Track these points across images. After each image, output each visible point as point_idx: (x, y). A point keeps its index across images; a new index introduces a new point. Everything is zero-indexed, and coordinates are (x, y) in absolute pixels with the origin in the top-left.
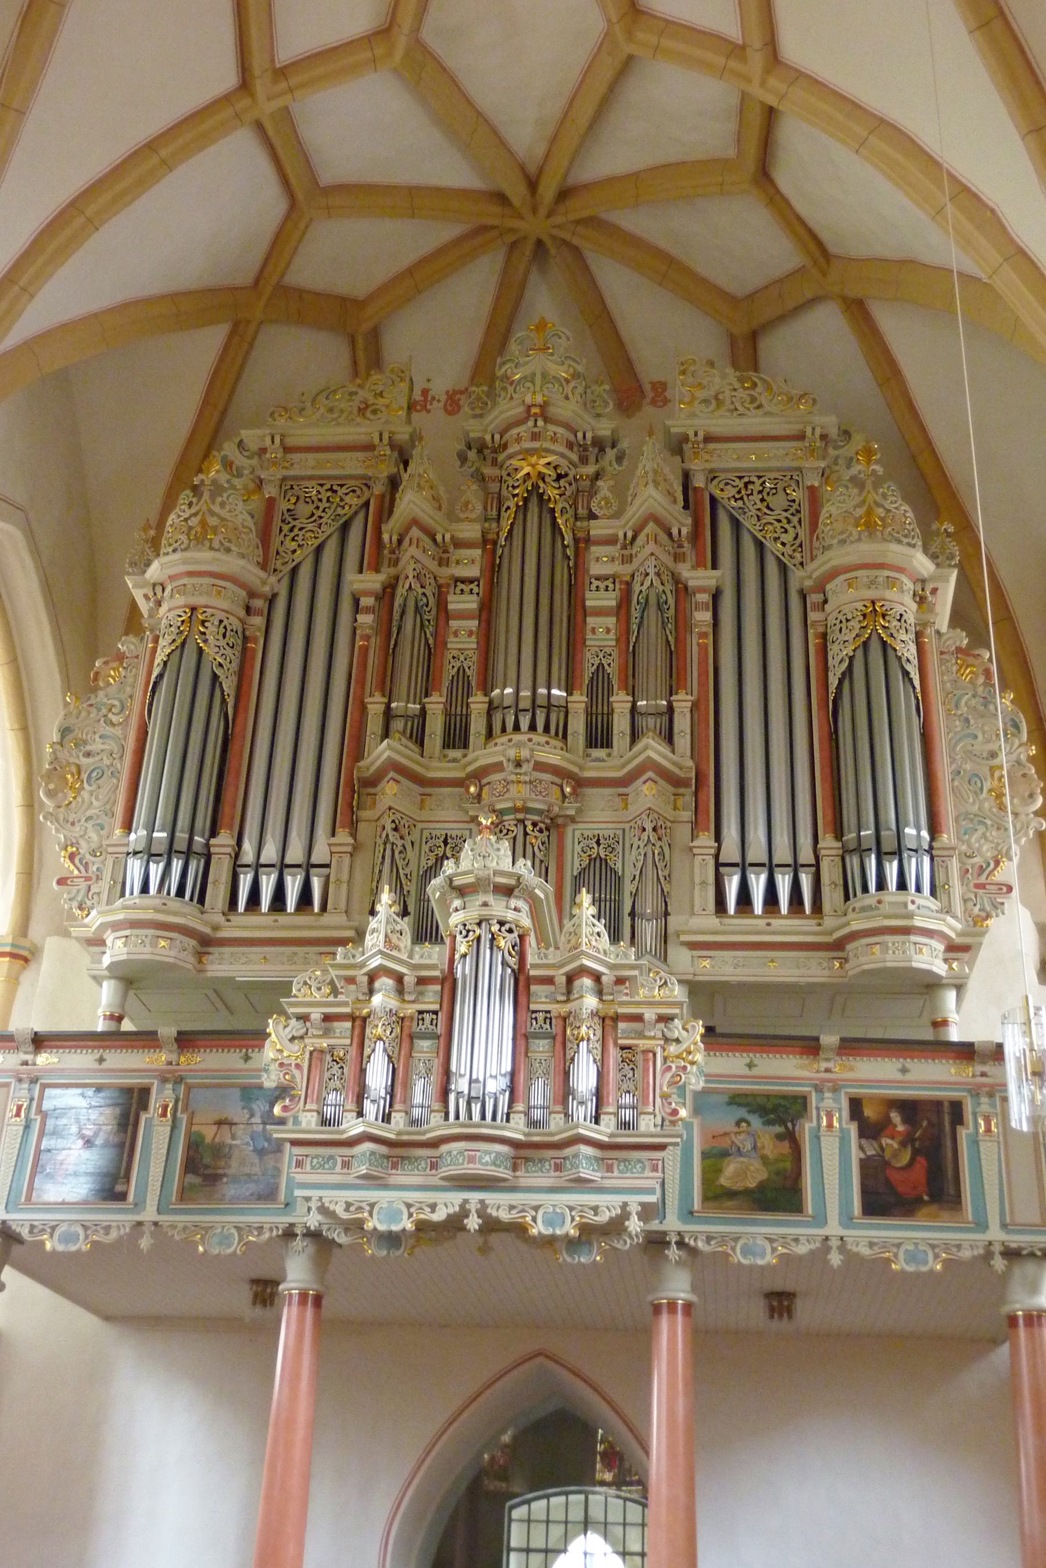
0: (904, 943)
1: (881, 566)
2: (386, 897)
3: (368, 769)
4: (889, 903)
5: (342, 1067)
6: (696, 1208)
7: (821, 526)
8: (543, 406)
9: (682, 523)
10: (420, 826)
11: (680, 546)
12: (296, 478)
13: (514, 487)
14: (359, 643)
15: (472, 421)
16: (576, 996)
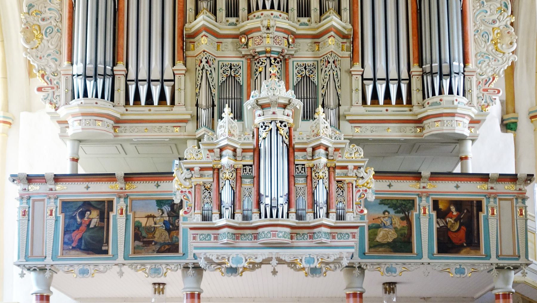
0: (452, 121)
2: (227, 110)
3: (191, 29)
4: (446, 101)
5: (210, 192)
6: (366, 251)
10: (218, 59)
16: (317, 157)
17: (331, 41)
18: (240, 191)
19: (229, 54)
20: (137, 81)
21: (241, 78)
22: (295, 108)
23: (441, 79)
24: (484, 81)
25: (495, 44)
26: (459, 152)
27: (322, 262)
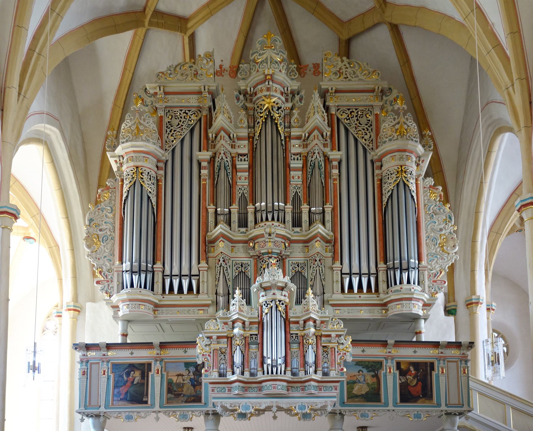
1: (405, 151)
2: (238, 292)
3: (211, 236)
9: (327, 131)
10: (232, 259)
12: (171, 107)
13: (261, 113)
14: (202, 183)
15: (241, 81)
17: (317, 244)
18: (248, 354)
19: (241, 255)
20: (171, 276)
22: (291, 290)
23: (401, 273)
24: (434, 274)
25: (442, 247)
26: (415, 328)
27: (311, 409)
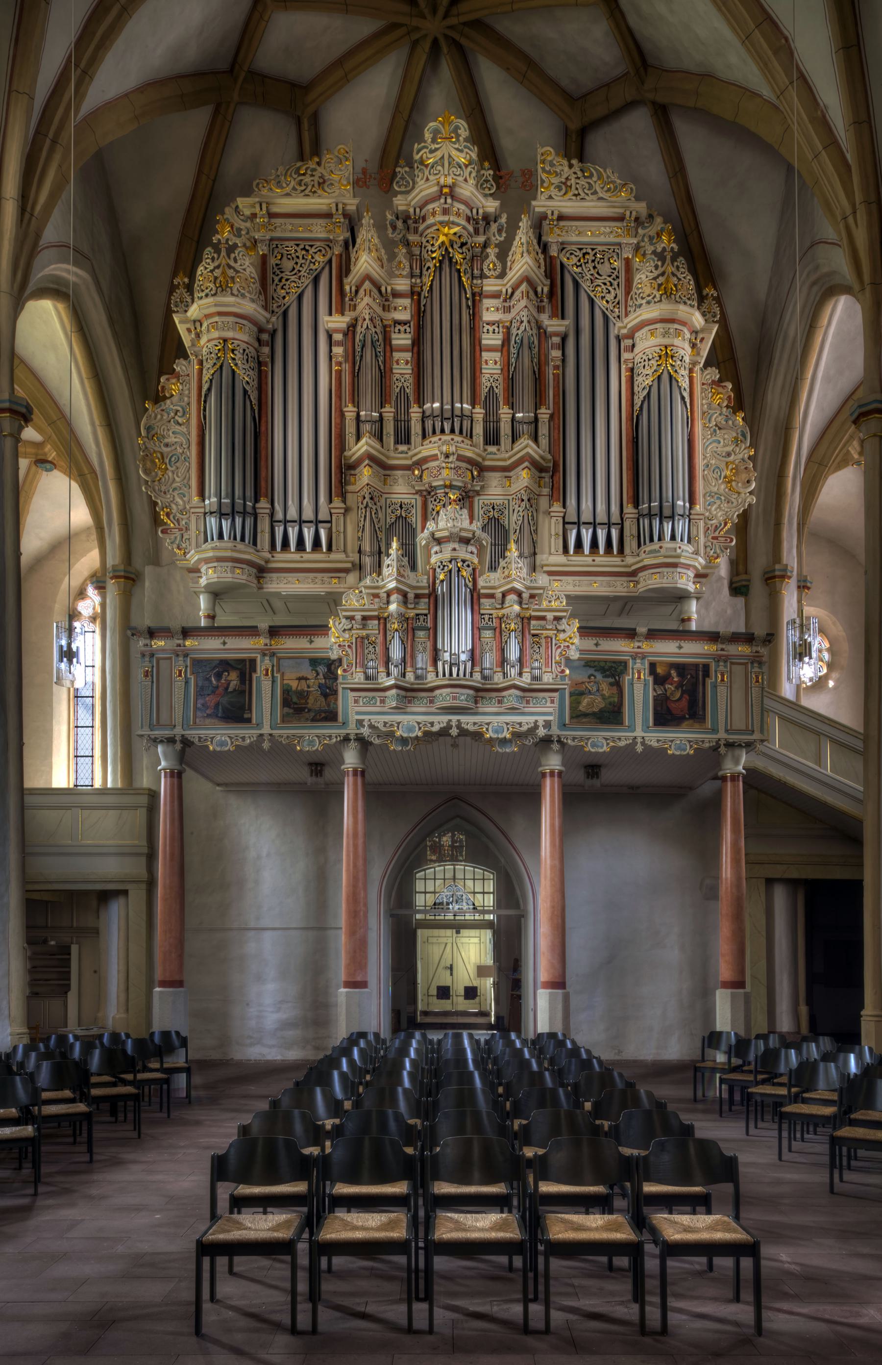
7: (634, 290)
8: (452, 187)
10: (385, 496)
11: (542, 301)
13: (433, 252)
20: (286, 522)
21: (414, 520)
23: (661, 523)
25: (729, 482)
26: (681, 612)
